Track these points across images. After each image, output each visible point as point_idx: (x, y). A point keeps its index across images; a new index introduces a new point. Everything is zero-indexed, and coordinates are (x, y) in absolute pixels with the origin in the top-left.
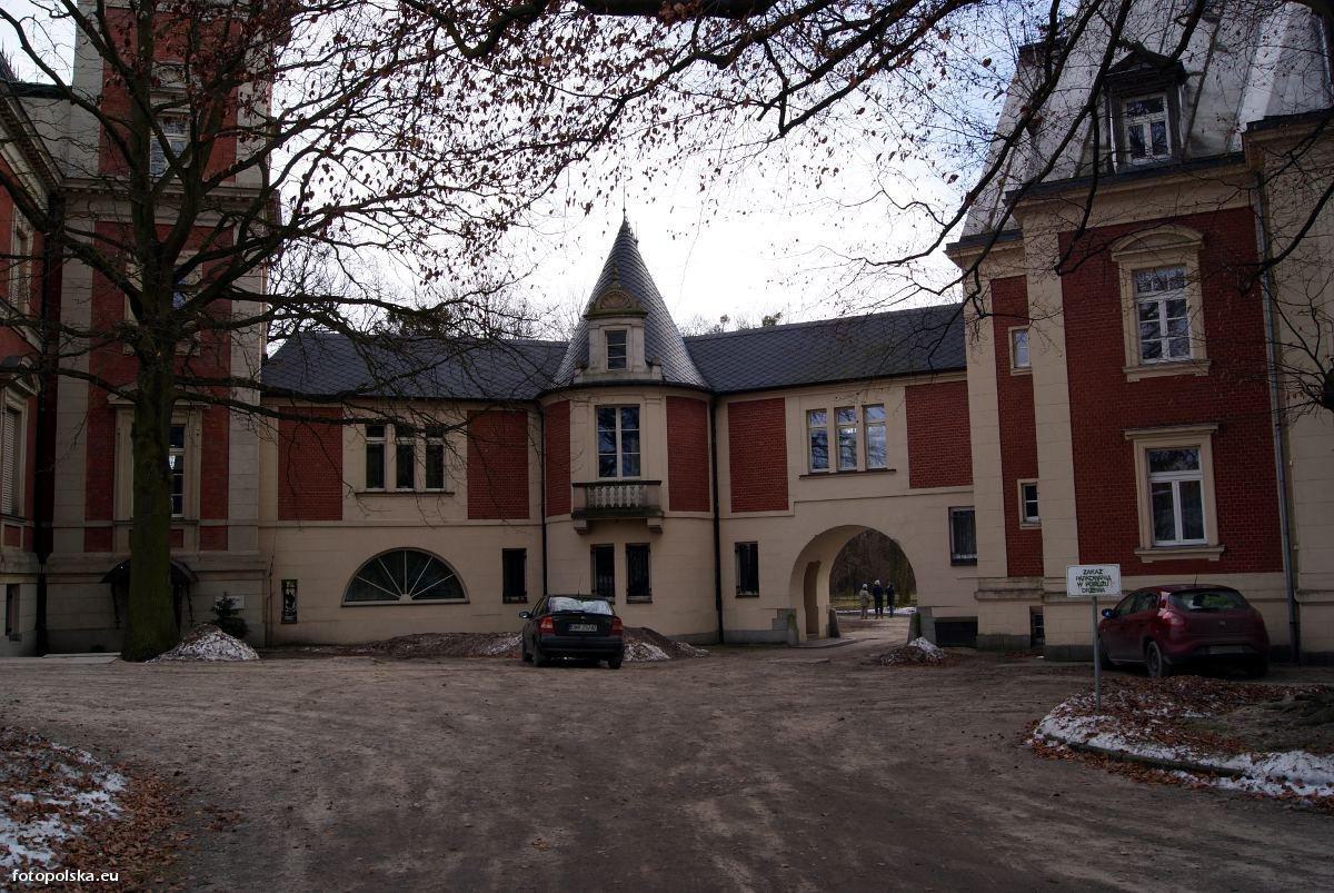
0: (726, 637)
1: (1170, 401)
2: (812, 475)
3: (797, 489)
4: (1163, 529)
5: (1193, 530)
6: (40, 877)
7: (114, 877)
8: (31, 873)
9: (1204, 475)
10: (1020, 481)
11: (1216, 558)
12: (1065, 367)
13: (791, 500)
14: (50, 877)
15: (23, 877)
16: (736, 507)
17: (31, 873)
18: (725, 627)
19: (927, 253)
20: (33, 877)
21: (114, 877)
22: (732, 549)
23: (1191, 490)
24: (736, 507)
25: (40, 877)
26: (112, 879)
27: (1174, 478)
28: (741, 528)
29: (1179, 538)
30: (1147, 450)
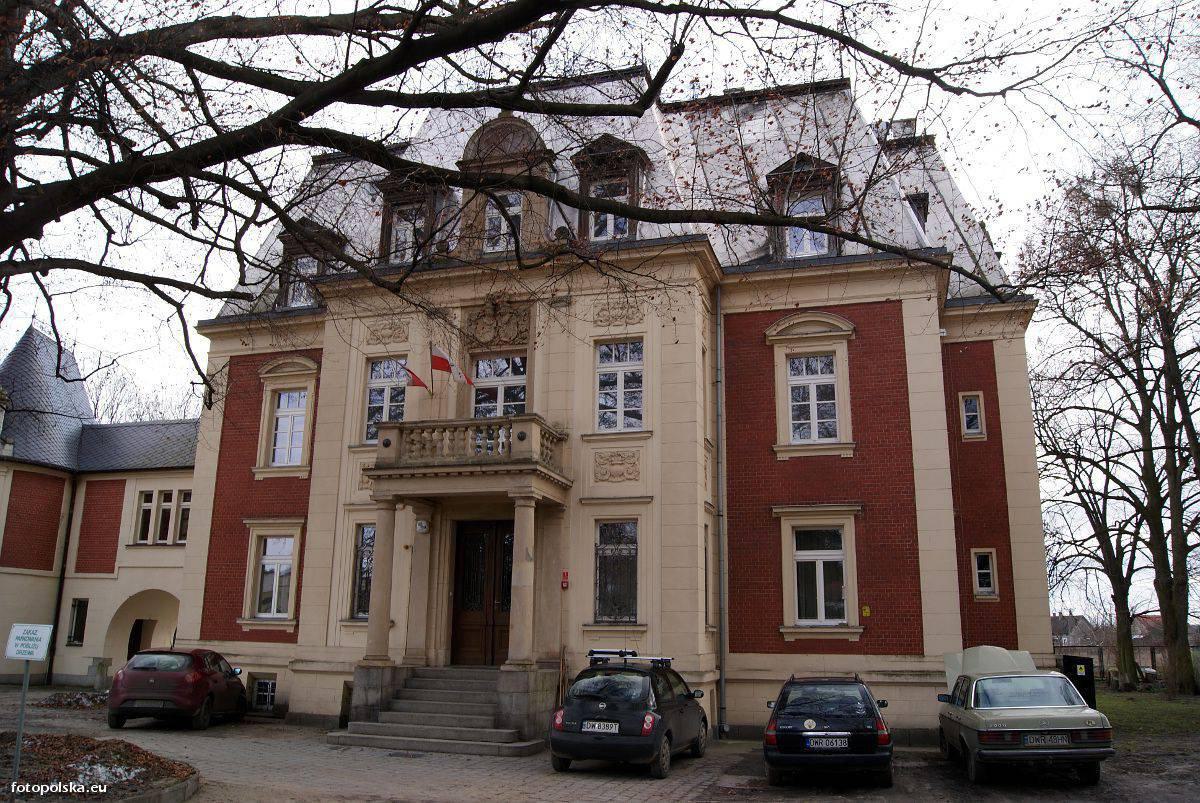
0: (54, 679)
1: (817, 478)
2: (136, 545)
3: (123, 556)
4: (807, 609)
5: (834, 612)
6: (36, 788)
7: (102, 788)
8: (28, 785)
9: (847, 555)
10: (973, 551)
11: (856, 639)
12: (218, 435)
13: (117, 565)
14: (45, 788)
16: (79, 569)
17: (28, 785)
18: (55, 671)
19: (255, 284)
20: (30, 788)
21: (102, 788)
22: (71, 602)
23: (834, 570)
24: (79, 569)
25: (36, 788)
26: (101, 791)
27: (820, 557)
28: (80, 586)
29: (821, 619)
30: (793, 527)
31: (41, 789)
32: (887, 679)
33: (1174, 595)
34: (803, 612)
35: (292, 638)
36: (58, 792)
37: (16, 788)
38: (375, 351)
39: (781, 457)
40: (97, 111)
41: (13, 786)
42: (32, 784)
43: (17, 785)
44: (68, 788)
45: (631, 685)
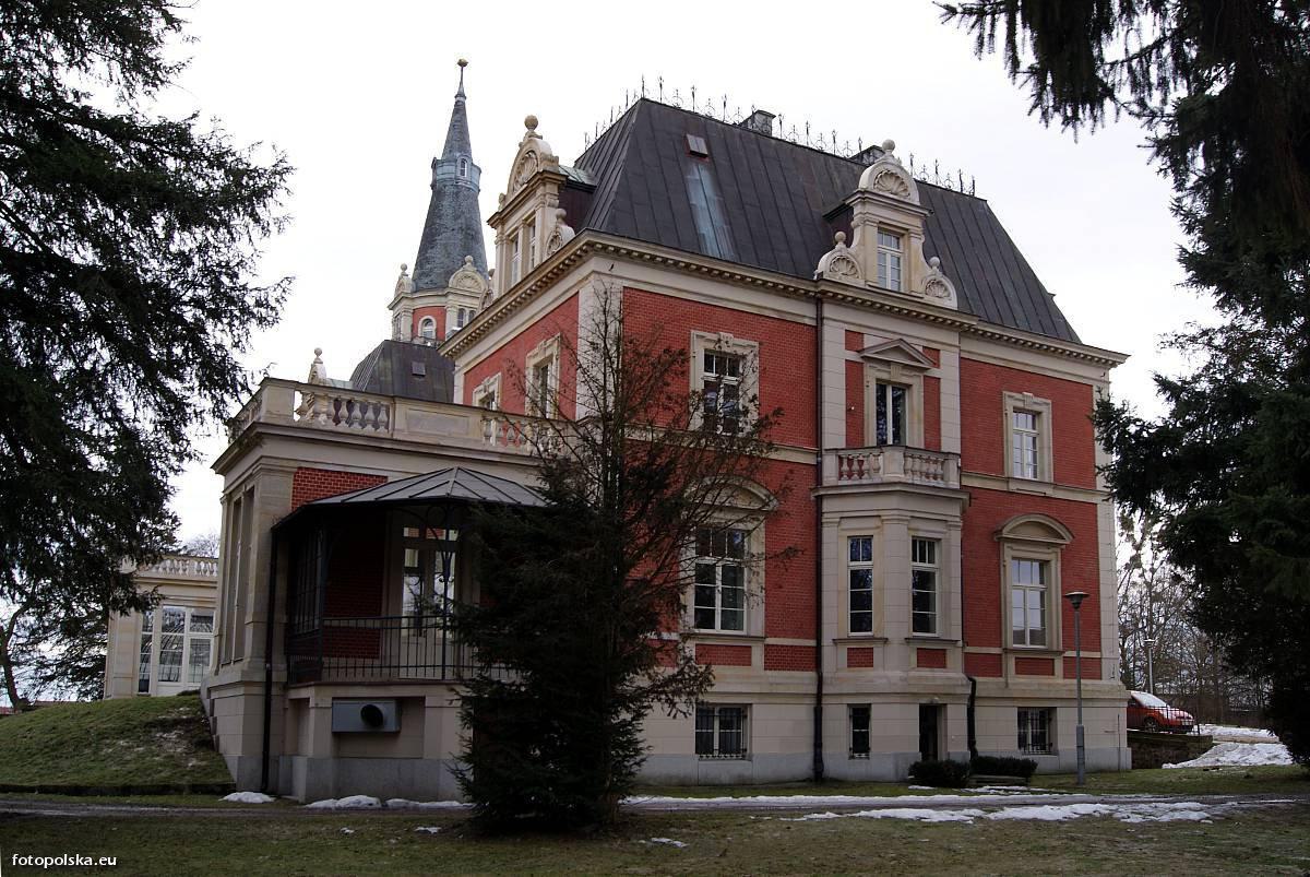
6: (39, 861)
7: (112, 861)
8: (30, 858)
14: (49, 861)
15: (23, 861)
17: (30, 858)
20: (33, 861)
21: (112, 861)
25: (39, 861)
31: (45, 862)
32: (789, 784)
33: (1040, 863)
34: (851, 336)
35: (334, 699)
36: (63, 865)
37: (17, 861)
38: (790, 453)
39: (1049, 401)
40: (659, 650)
41: (14, 858)
42: (35, 856)
43: (19, 857)
44: (75, 860)
45: (693, 173)
